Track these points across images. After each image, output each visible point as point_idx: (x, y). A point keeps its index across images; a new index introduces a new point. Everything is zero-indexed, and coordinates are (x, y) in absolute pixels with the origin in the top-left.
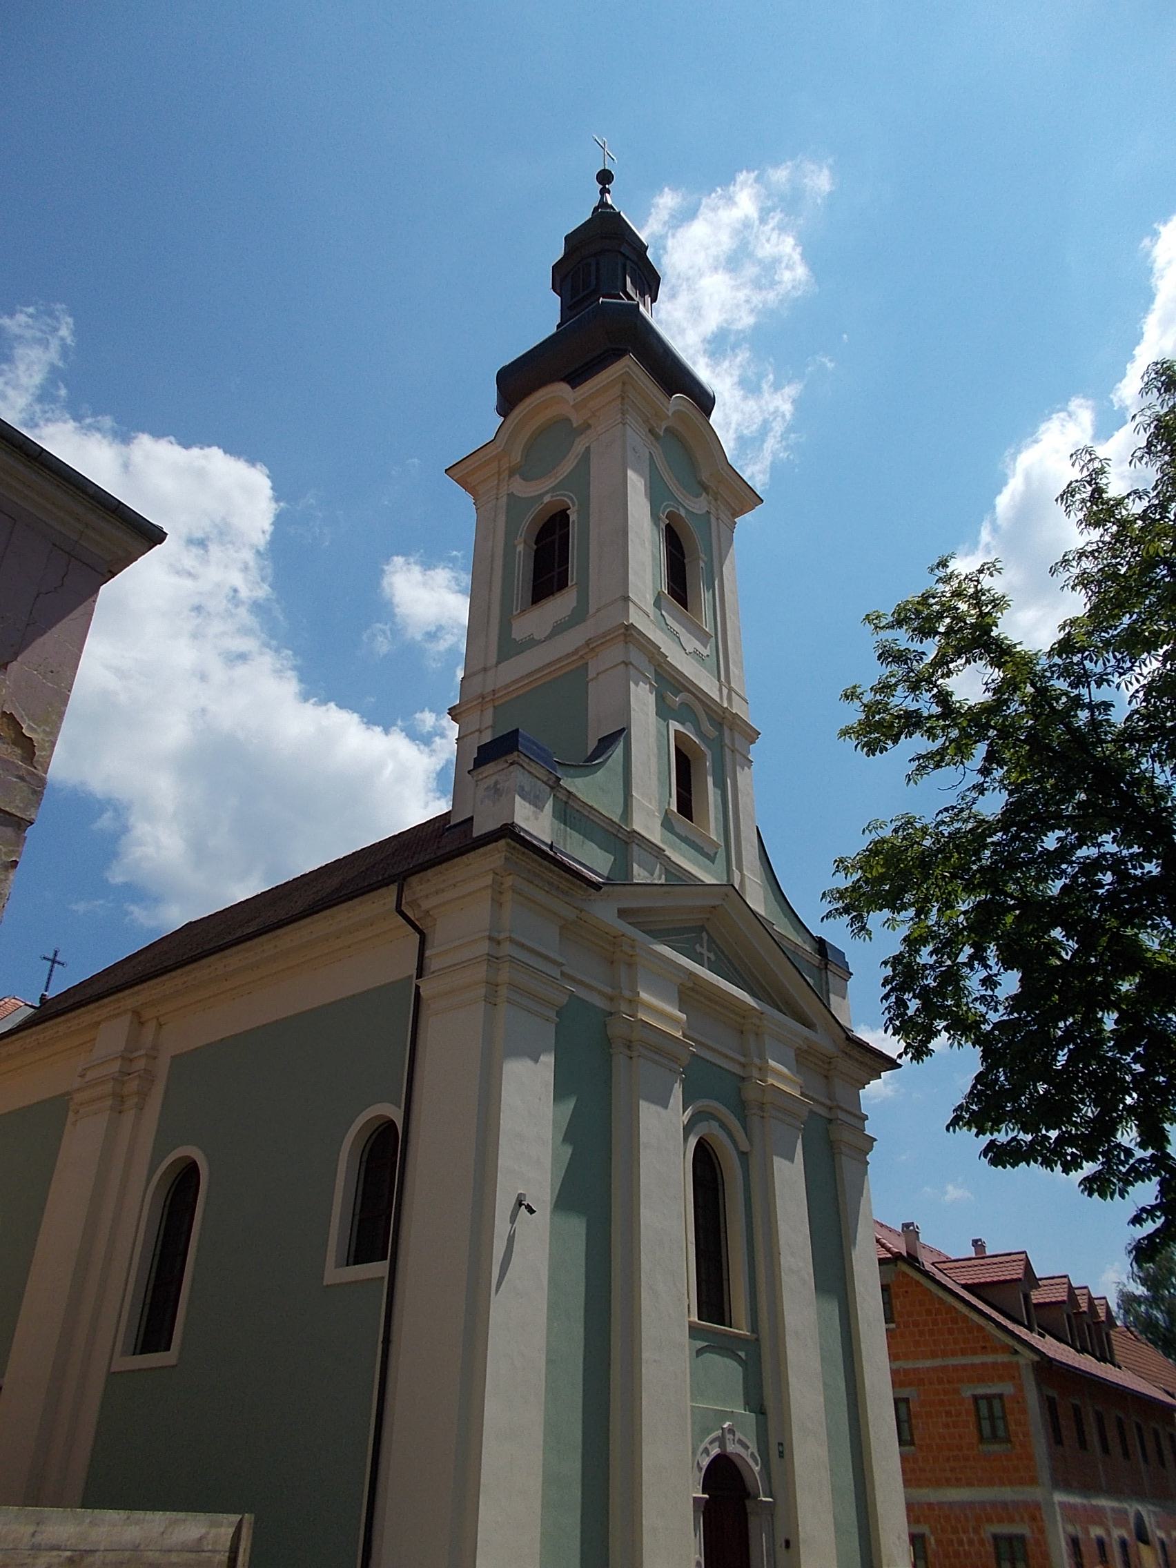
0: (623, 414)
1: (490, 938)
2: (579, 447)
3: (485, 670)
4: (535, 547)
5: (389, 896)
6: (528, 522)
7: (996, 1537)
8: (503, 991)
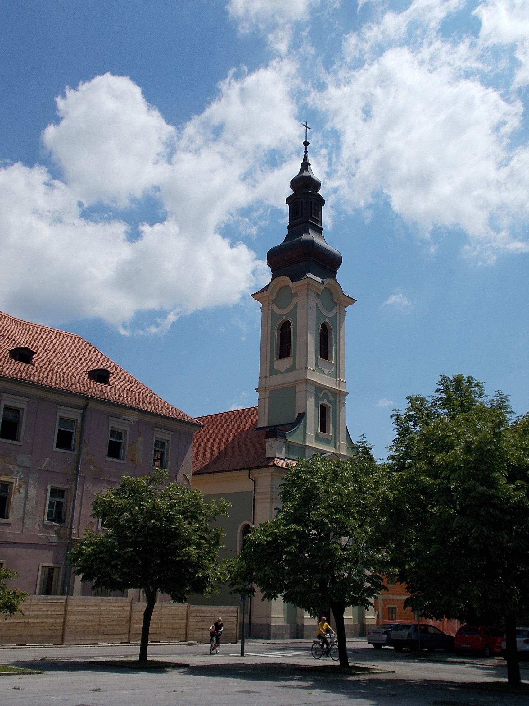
0: (308, 295)
1: (271, 488)
2: (295, 301)
3: (266, 377)
4: (280, 332)
5: (248, 471)
6: (279, 323)
7: (389, 608)
8: (274, 500)
